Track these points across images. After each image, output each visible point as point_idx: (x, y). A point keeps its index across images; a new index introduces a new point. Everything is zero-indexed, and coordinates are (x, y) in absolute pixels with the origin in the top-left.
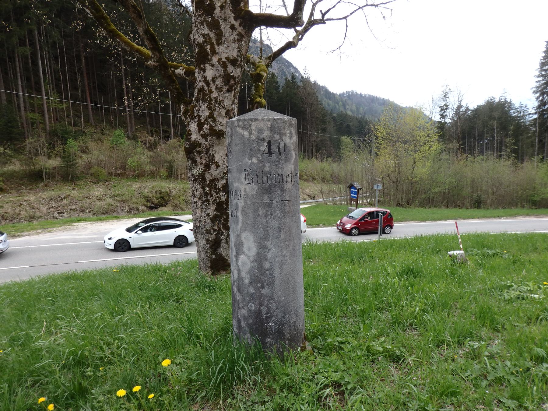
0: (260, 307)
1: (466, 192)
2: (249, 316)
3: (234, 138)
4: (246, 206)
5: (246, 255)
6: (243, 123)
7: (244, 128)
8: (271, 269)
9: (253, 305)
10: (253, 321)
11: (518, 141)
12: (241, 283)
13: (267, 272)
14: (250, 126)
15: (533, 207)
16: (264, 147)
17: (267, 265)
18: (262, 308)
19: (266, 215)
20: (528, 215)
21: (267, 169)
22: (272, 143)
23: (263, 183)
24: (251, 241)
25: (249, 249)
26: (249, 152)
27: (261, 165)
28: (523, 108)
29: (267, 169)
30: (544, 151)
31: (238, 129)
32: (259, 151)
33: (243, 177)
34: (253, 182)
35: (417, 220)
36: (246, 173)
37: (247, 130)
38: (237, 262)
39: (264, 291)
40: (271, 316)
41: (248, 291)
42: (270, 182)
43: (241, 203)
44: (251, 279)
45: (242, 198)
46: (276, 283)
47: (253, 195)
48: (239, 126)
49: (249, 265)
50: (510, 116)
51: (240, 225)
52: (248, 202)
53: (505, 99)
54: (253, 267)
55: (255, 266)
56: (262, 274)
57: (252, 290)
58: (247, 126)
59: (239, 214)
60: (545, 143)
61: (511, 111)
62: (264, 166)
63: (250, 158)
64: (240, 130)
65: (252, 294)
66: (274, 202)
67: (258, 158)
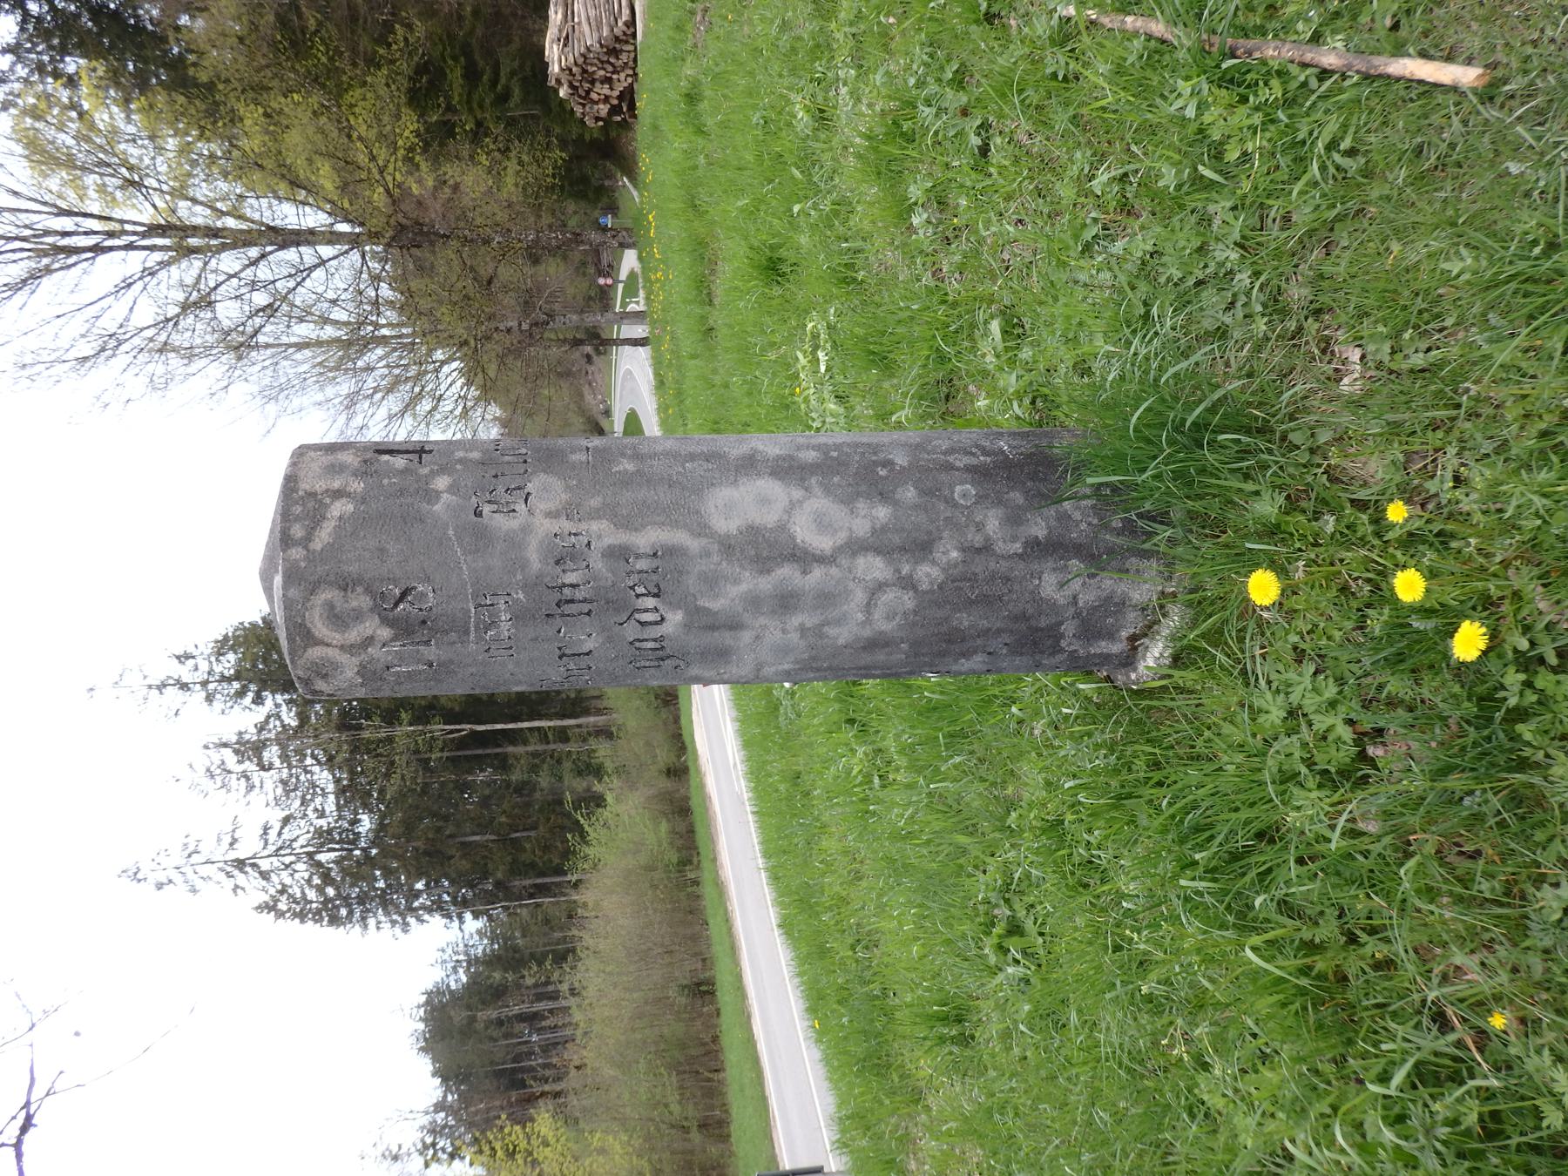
0: (958, 469)
2: (999, 502)
3: (353, 569)
4: (609, 512)
6: (297, 519)
7: (315, 519)
9: (958, 489)
10: (1012, 489)
11: (532, 956)
12: (897, 540)
14: (312, 495)
15: (695, 860)
20: (714, 860)
31: (317, 545)
33: (502, 523)
35: (763, 1091)
36: (486, 509)
37: (327, 506)
38: (821, 559)
41: (916, 507)
42: (524, 451)
43: (603, 533)
44: (868, 497)
45: (583, 526)
47: (568, 488)
48: (308, 538)
49: (819, 503)
50: (467, 987)
51: (680, 537)
53: (419, 1007)
54: (828, 490)
57: (909, 494)
61: (453, 986)
64: (324, 535)
65: (923, 492)
67: (433, 474)
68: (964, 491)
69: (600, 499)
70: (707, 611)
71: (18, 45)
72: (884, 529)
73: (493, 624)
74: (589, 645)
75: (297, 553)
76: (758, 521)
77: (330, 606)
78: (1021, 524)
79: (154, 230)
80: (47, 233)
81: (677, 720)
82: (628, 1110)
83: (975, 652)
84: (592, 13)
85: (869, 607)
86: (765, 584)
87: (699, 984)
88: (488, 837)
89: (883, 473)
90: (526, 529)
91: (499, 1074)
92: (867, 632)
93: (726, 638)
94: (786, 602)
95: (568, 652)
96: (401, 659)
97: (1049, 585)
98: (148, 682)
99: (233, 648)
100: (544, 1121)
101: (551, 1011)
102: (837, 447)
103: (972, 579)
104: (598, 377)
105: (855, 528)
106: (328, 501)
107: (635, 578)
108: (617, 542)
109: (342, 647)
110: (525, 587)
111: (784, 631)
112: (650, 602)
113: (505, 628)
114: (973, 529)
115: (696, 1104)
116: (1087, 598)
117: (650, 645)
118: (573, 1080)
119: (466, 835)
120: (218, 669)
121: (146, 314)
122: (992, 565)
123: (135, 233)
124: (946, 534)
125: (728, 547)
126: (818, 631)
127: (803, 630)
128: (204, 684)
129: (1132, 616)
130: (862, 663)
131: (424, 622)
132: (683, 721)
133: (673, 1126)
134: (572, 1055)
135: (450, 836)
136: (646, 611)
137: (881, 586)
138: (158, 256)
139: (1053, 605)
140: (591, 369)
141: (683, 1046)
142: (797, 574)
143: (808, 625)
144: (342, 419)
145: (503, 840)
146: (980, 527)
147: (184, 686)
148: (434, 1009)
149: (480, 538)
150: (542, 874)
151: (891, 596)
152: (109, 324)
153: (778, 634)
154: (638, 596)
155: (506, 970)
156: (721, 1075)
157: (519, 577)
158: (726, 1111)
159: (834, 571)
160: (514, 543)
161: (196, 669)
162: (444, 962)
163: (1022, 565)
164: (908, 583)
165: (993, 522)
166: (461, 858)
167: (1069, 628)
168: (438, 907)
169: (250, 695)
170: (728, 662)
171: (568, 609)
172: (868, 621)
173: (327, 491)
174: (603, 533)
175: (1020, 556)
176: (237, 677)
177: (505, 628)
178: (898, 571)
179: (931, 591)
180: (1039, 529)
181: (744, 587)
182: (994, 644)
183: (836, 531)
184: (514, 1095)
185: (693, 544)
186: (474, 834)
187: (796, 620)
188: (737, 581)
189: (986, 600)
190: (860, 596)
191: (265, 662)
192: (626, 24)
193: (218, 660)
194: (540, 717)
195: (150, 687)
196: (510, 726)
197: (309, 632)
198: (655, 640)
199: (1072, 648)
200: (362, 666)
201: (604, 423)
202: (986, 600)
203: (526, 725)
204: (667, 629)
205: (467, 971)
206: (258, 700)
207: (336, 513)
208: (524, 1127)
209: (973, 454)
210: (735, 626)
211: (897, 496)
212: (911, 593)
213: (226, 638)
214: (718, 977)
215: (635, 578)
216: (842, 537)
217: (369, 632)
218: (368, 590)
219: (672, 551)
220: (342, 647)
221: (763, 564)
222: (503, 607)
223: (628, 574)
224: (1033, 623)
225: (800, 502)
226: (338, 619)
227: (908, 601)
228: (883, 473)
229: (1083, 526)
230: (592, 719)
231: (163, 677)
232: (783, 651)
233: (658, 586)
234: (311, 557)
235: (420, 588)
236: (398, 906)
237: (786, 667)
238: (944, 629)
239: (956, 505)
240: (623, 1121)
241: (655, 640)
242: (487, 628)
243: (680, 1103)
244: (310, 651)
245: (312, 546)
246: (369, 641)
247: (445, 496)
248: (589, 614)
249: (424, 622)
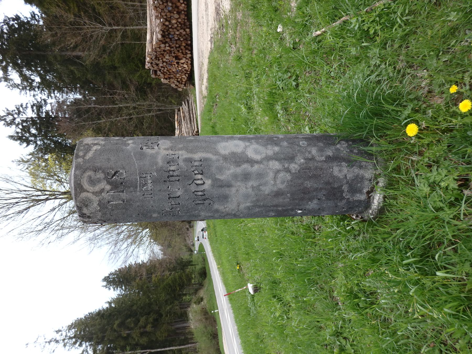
3: (99, 165)
9: (301, 142)
10: (319, 142)
12: (282, 156)
14: (88, 144)
31: (87, 158)
33: (150, 151)
36: (144, 148)
38: (257, 162)
43: (184, 154)
44: (272, 144)
45: (177, 152)
47: (171, 143)
48: (85, 155)
49: (255, 146)
51: (209, 155)
52: (181, 146)
54: (258, 143)
64: (90, 154)
69: (182, 145)
70: (219, 179)
71: (34, 153)
72: (278, 153)
73: (146, 184)
74: (179, 193)
76: (235, 151)
77: (90, 177)
78: (323, 151)
79: (65, 193)
80: (33, 196)
81: (218, 343)
83: (314, 199)
84: (187, 130)
85: (275, 178)
86: (239, 170)
90: (157, 153)
92: (275, 189)
95: (172, 196)
97: (336, 171)
98: (46, 340)
99: (74, 328)
103: (309, 169)
104: (190, 234)
105: (268, 153)
106: (91, 129)
109: (93, 193)
110: (157, 171)
111: (246, 188)
112: (199, 176)
113: (150, 186)
116: (349, 176)
117: (200, 193)
120: (69, 334)
121: (59, 215)
122: (316, 164)
123: (58, 194)
124: (298, 154)
125: (225, 158)
127: (253, 187)
128: (64, 340)
129: (367, 183)
130: (274, 203)
131: (122, 183)
132: (220, 343)
136: (198, 179)
137: (278, 171)
138: (64, 201)
140: (188, 232)
142: (249, 167)
143: (255, 186)
144: (113, 247)
146: (310, 152)
147: (57, 341)
151: (282, 174)
152: (47, 220)
153: (244, 189)
154: (195, 174)
159: (262, 166)
160: (154, 157)
161: (62, 335)
163: (326, 164)
164: (288, 170)
165: (314, 151)
167: (345, 188)
169: (78, 343)
170: (227, 202)
171: (172, 179)
172: (275, 184)
174: (184, 154)
175: (325, 161)
176: (74, 337)
177: (150, 186)
178: (284, 166)
179: (295, 173)
180: (330, 153)
181: (232, 171)
182: (320, 195)
185: (214, 157)
187: (250, 184)
188: (229, 169)
189: (315, 177)
190: (271, 175)
191: (84, 332)
192: (196, 132)
193: (69, 332)
194: (173, 346)
195: (46, 342)
196: (163, 349)
197: (82, 186)
198: (201, 191)
199: (347, 197)
200: (100, 201)
201: (192, 248)
202: (315, 177)
203: (168, 349)
204: (206, 187)
206: (81, 345)
210: (229, 186)
212: (289, 174)
213: (72, 324)
216: (264, 155)
217: (103, 187)
218: (103, 172)
219: (206, 160)
220: (93, 193)
222: (149, 178)
223: (192, 167)
224: (332, 185)
226: (92, 182)
227: (288, 177)
229: (345, 152)
230: (190, 345)
231: (51, 338)
232: (247, 196)
233: (202, 171)
234: (85, 161)
235: (121, 171)
237: (248, 204)
238: (302, 187)
239: (301, 146)
241: (201, 191)
242: (144, 186)
244: (82, 194)
245: (85, 158)
246: (102, 190)
248: (179, 180)
249: (122, 183)
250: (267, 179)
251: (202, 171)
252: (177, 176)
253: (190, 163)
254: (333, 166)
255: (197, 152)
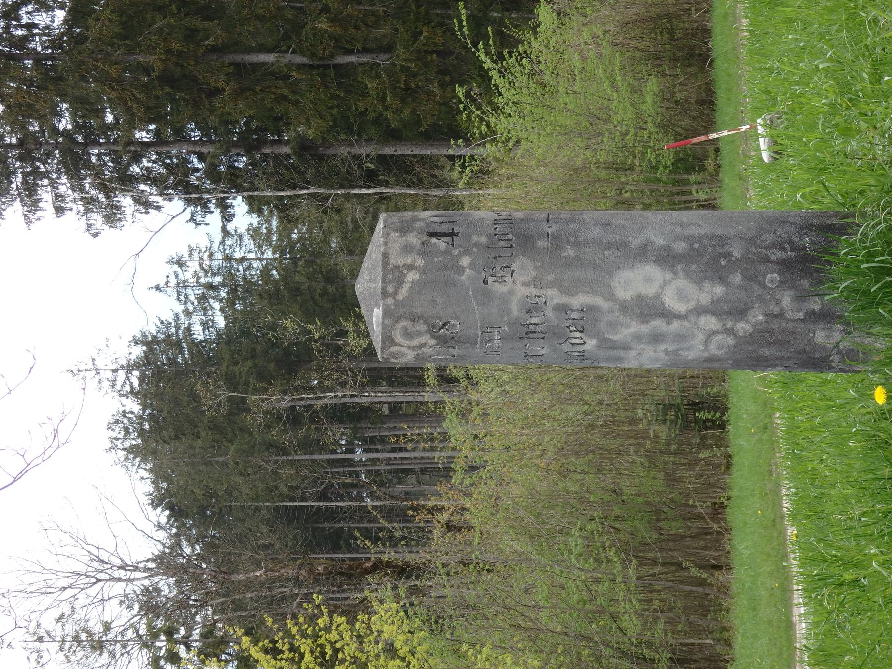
0: (771, 262)
1: (639, 480)
2: (793, 287)
3: (419, 311)
4: (557, 284)
5: (662, 288)
7: (400, 282)
8: (688, 239)
9: (769, 276)
10: (803, 277)
12: (726, 307)
13: (696, 246)
14: (397, 267)
15: (710, 164)
16: (441, 244)
17: (681, 247)
18: (773, 258)
19: (577, 244)
21: (483, 240)
22: (431, 230)
23: (512, 247)
24: (632, 275)
25: (648, 280)
26: (449, 272)
27: (475, 250)
28: (188, 276)
29: (483, 240)
30: (422, 159)
31: (400, 297)
32: (446, 252)
34: (508, 267)
36: (490, 280)
37: (405, 275)
38: (679, 317)
39: (737, 253)
40: (790, 242)
42: (510, 236)
43: (554, 296)
45: (543, 292)
46: (719, 232)
47: (536, 268)
48: (396, 293)
49: (682, 283)
50: (226, 339)
51: (598, 301)
52: (550, 277)
53: (129, 368)
55: (684, 270)
56: (701, 255)
57: (737, 278)
58: (397, 274)
59: (578, 301)
60: (382, 159)
62: (476, 245)
63: (460, 270)
64: (404, 292)
65: (746, 278)
66: (550, 231)
67: (461, 255)
68: (772, 277)
70: (611, 340)
72: (719, 301)
75: (390, 301)
82: (544, 615)
85: (706, 343)
86: (645, 328)
87: (696, 406)
88: (290, 58)
89: (723, 263)
90: (511, 293)
91: (292, 516)
92: (706, 355)
93: (622, 353)
94: (656, 338)
96: (438, 353)
100: (387, 617)
101: (395, 408)
102: (700, 239)
103: (771, 331)
106: (405, 271)
107: (570, 322)
108: (561, 302)
109: (409, 348)
111: (655, 352)
112: (578, 335)
113: (496, 342)
114: (774, 303)
115: (670, 622)
117: (577, 354)
118: (440, 548)
119: (250, 50)
122: (784, 324)
124: (756, 305)
125: (624, 307)
126: (676, 352)
127: (666, 352)
133: (624, 654)
134: (443, 498)
135: (214, 49)
137: (714, 333)
139: (823, 348)
141: (656, 514)
142: (664, 324)
145: (320, 68)
146: (778, 302)
148: (159, 373)
149: (486, 297)
150: (394, 135)
153: (652, 353)
154: (571, 331)
155: (309, 317)
156: (721, 577)
157: (506, 319)
158: (728, 643)
159: (686, 323)
160: (505, 300)
162: (182, 285)
163: (802, 325)
166: (237, 94)
168: (176, 181)
172: (706, 349)
173: (405, 265)
175: (802, 320)
177: (496, 342)
178: (725, 325)
179: (745, 337)
180: (815, 305)
181: (632, 330)
183: (689, 301)
184: (321, 561)
186: (263, 49)
187: (662, 347)
188: (628, 326)
190: (701, 337)
202: (778, 343)
204: (587, 347)
205: (228, 305)
207: (410, 280)
208: (352, 622)
209: (784, 249)
210: (626, 348)
211: (730, 280)
214: (734, 399)
215: (570, 322)
216: (692, 305)
218: (425, 322)
220: (409, 348)
221: (644, 317)
223: (567, 320)
225: (669, 281)
226: (408, 335)
227: (731, 341)
228: (723, 263)
233: (583, 327)
234: (397, 304)
235: (453, 322)
236: (109, 180)
238: (754, 355)
239: (765, 287)
240: (534, 634)
243: (640, 615)
245: (397, 298)
246: (424, 345)
247: (468, 270)
250: (692, 342)
251: (583, 327)
252: (541, 332)
253: (564, 314)
254: (815, 330)
255: (577, 293)
